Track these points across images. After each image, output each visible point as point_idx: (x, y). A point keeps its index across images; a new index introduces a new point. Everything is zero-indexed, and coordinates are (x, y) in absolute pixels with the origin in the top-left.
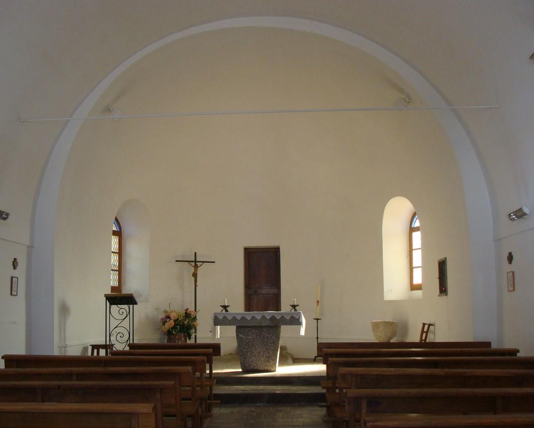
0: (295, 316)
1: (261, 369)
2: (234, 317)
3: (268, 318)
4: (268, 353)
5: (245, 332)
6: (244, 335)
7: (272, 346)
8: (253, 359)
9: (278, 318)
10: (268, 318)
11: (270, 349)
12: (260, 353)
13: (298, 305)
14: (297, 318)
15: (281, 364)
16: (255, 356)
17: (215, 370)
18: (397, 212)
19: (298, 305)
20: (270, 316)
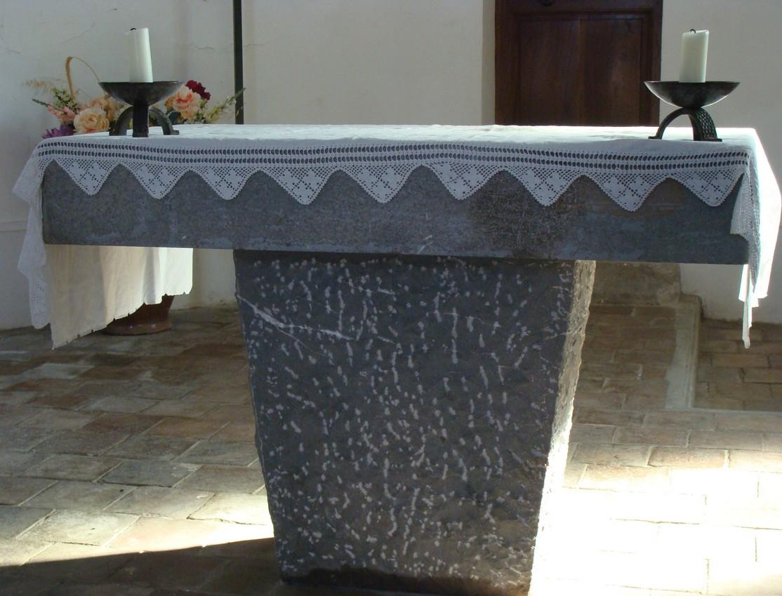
0: (695, 184)
1: (415, 570)
2: (259, 176)
3: (459, 190)
4: (473, 456)
5: (298, 294)
6: (292, 316)
7: (499, 411)
8: (357, 498)
9: (545, 198)
10: (459, 190)
11: (487, 431)
12: (407, 455)
13: (727, 87)
14: (713, 198)
15: (502, 368)
16: (371, 474)
17: (700, 77)
18: (328, 378)
19: (727, 87)
20: (477, 180)
